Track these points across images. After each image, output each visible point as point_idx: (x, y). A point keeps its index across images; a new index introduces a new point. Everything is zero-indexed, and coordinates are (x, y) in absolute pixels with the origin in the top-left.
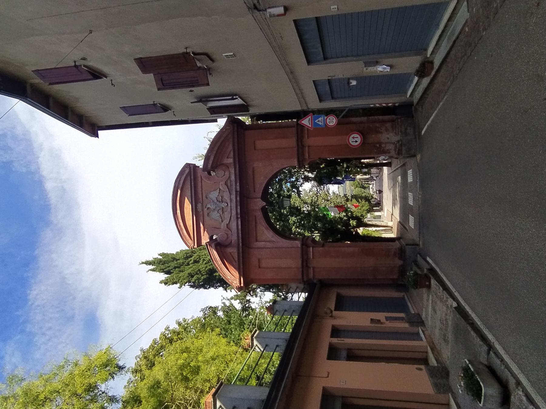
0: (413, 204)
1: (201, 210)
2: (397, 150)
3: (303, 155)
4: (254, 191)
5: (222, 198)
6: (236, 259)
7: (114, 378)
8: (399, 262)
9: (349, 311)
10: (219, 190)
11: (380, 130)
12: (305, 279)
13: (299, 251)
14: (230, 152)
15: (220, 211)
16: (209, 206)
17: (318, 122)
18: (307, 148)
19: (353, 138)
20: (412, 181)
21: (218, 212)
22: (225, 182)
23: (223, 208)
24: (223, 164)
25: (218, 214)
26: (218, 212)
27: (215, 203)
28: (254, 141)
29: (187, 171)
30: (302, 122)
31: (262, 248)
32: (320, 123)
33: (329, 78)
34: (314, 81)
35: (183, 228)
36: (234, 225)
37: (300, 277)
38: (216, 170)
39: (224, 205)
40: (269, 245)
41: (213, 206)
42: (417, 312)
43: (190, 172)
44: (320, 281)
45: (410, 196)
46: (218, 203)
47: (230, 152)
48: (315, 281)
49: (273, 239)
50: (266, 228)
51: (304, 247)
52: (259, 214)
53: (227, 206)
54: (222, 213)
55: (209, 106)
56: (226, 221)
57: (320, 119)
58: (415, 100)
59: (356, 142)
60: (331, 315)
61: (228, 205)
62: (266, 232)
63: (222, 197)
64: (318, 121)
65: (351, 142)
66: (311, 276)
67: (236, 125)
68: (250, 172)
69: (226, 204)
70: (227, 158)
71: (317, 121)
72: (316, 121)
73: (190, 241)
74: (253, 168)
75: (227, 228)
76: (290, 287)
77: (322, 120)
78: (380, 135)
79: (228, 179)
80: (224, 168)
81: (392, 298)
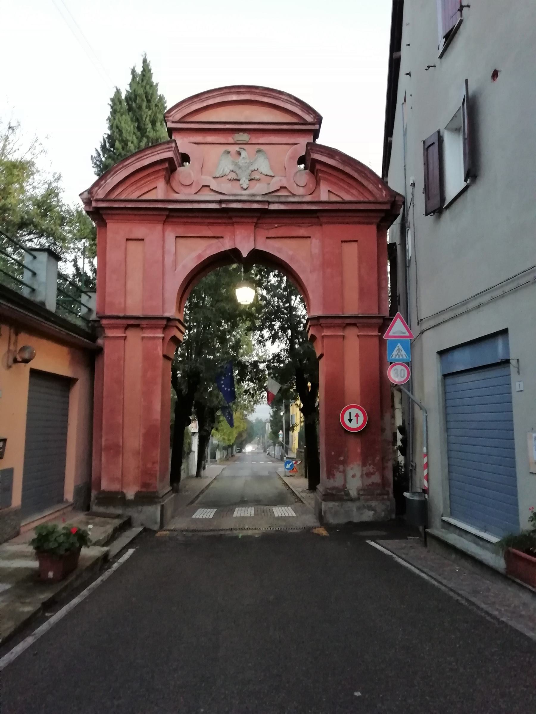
0: (237, 517)
1: (236, 139)
2: (334, 492)
3: (329, 327)
4: (267, 238)
5: (257, 180)
6: (144, 197)
7: (91, 270)
8: (130, 494)
9: (30, 398)
10: (271, 176)
11: (370, 462)
12: (104, 322)
13: (158, 314)
14: (339, 196)
15: (233, 176)
16: (244, 154)
17: (397, 348)
18: (341, 334)
19: (357, 416)
20: (276, 515)
21: (232, 171)
22: (285, 188)
23: (239, 180)
24: (318, 183)
25: (228, 171)
26: (232, 171)
27: (249, 167)
28: (356, 241)
29: (309, 118)
30: (399, 319)
31: (163, 247)
32: (395, 353)
33: (513, 362)
34: (504, 332)
35: (205, 104)
36: (207, 196)
37: (108, 313)
38: (307, 171)
39: (244, 182)
40: (169, 260)
41: (243, 161)
42: (22, 530)
43: (306, 123)
44: (100, 350)
45: (249, 511)
46: (249, 171)
47: (339, 196)
48: (100, 341)
49: (179, 268)
50: (199, 256)
51: (165, 322)
52: (226, 245)
53: (242, 187)
54: (229, 177)
55: (443, 133)
56: (214, 185)
57: (403, 353)
58: (437, 530)
59: (350, 420)
60: (19, 359)
61: (245, 190)
62: (194, 254)
63: (258, 180)
64: (399, 349)
65: (350, 410)
66: (110, 333)
67: (387, 207)
68: (302, 232)
69: (245, 187)
70: (329, 191)
71: (401, 347)
72: (399, 345)
73: (178, 117)
74: (310, 237)
75: (203, 186)
76: (90, 297)
77: (402, 355)
78: (360, 463)
79: (290, 192)
80: (311, 185)
81: (62, 479)
